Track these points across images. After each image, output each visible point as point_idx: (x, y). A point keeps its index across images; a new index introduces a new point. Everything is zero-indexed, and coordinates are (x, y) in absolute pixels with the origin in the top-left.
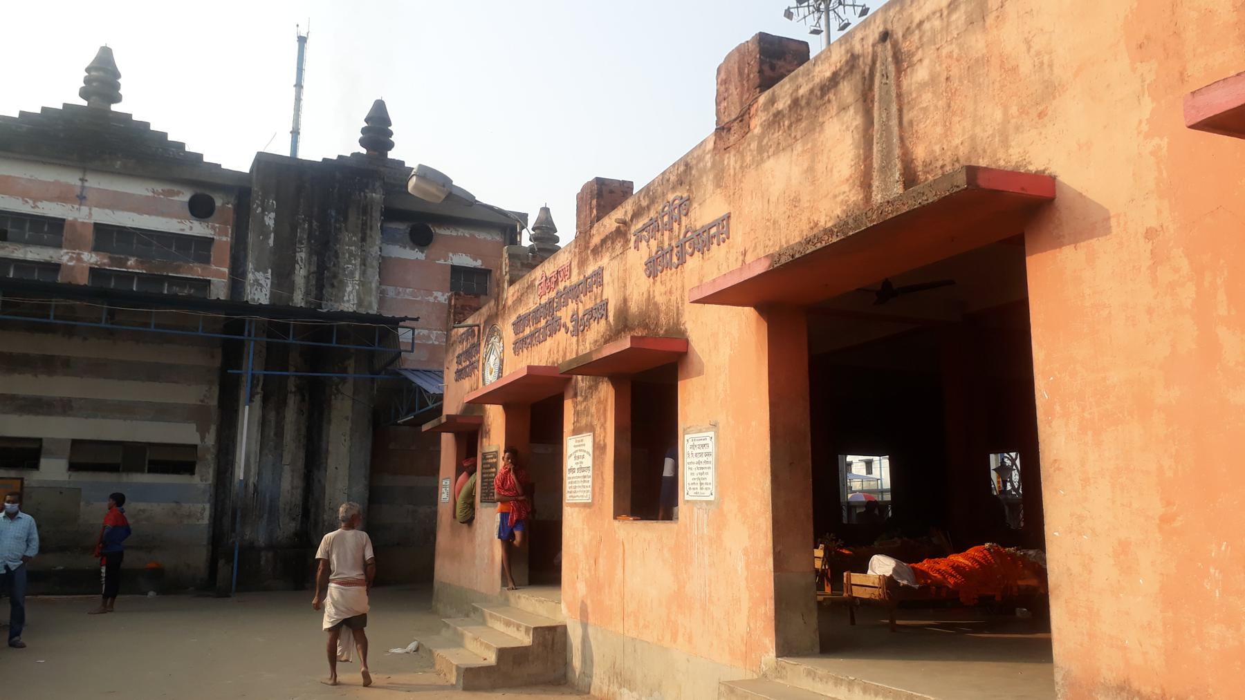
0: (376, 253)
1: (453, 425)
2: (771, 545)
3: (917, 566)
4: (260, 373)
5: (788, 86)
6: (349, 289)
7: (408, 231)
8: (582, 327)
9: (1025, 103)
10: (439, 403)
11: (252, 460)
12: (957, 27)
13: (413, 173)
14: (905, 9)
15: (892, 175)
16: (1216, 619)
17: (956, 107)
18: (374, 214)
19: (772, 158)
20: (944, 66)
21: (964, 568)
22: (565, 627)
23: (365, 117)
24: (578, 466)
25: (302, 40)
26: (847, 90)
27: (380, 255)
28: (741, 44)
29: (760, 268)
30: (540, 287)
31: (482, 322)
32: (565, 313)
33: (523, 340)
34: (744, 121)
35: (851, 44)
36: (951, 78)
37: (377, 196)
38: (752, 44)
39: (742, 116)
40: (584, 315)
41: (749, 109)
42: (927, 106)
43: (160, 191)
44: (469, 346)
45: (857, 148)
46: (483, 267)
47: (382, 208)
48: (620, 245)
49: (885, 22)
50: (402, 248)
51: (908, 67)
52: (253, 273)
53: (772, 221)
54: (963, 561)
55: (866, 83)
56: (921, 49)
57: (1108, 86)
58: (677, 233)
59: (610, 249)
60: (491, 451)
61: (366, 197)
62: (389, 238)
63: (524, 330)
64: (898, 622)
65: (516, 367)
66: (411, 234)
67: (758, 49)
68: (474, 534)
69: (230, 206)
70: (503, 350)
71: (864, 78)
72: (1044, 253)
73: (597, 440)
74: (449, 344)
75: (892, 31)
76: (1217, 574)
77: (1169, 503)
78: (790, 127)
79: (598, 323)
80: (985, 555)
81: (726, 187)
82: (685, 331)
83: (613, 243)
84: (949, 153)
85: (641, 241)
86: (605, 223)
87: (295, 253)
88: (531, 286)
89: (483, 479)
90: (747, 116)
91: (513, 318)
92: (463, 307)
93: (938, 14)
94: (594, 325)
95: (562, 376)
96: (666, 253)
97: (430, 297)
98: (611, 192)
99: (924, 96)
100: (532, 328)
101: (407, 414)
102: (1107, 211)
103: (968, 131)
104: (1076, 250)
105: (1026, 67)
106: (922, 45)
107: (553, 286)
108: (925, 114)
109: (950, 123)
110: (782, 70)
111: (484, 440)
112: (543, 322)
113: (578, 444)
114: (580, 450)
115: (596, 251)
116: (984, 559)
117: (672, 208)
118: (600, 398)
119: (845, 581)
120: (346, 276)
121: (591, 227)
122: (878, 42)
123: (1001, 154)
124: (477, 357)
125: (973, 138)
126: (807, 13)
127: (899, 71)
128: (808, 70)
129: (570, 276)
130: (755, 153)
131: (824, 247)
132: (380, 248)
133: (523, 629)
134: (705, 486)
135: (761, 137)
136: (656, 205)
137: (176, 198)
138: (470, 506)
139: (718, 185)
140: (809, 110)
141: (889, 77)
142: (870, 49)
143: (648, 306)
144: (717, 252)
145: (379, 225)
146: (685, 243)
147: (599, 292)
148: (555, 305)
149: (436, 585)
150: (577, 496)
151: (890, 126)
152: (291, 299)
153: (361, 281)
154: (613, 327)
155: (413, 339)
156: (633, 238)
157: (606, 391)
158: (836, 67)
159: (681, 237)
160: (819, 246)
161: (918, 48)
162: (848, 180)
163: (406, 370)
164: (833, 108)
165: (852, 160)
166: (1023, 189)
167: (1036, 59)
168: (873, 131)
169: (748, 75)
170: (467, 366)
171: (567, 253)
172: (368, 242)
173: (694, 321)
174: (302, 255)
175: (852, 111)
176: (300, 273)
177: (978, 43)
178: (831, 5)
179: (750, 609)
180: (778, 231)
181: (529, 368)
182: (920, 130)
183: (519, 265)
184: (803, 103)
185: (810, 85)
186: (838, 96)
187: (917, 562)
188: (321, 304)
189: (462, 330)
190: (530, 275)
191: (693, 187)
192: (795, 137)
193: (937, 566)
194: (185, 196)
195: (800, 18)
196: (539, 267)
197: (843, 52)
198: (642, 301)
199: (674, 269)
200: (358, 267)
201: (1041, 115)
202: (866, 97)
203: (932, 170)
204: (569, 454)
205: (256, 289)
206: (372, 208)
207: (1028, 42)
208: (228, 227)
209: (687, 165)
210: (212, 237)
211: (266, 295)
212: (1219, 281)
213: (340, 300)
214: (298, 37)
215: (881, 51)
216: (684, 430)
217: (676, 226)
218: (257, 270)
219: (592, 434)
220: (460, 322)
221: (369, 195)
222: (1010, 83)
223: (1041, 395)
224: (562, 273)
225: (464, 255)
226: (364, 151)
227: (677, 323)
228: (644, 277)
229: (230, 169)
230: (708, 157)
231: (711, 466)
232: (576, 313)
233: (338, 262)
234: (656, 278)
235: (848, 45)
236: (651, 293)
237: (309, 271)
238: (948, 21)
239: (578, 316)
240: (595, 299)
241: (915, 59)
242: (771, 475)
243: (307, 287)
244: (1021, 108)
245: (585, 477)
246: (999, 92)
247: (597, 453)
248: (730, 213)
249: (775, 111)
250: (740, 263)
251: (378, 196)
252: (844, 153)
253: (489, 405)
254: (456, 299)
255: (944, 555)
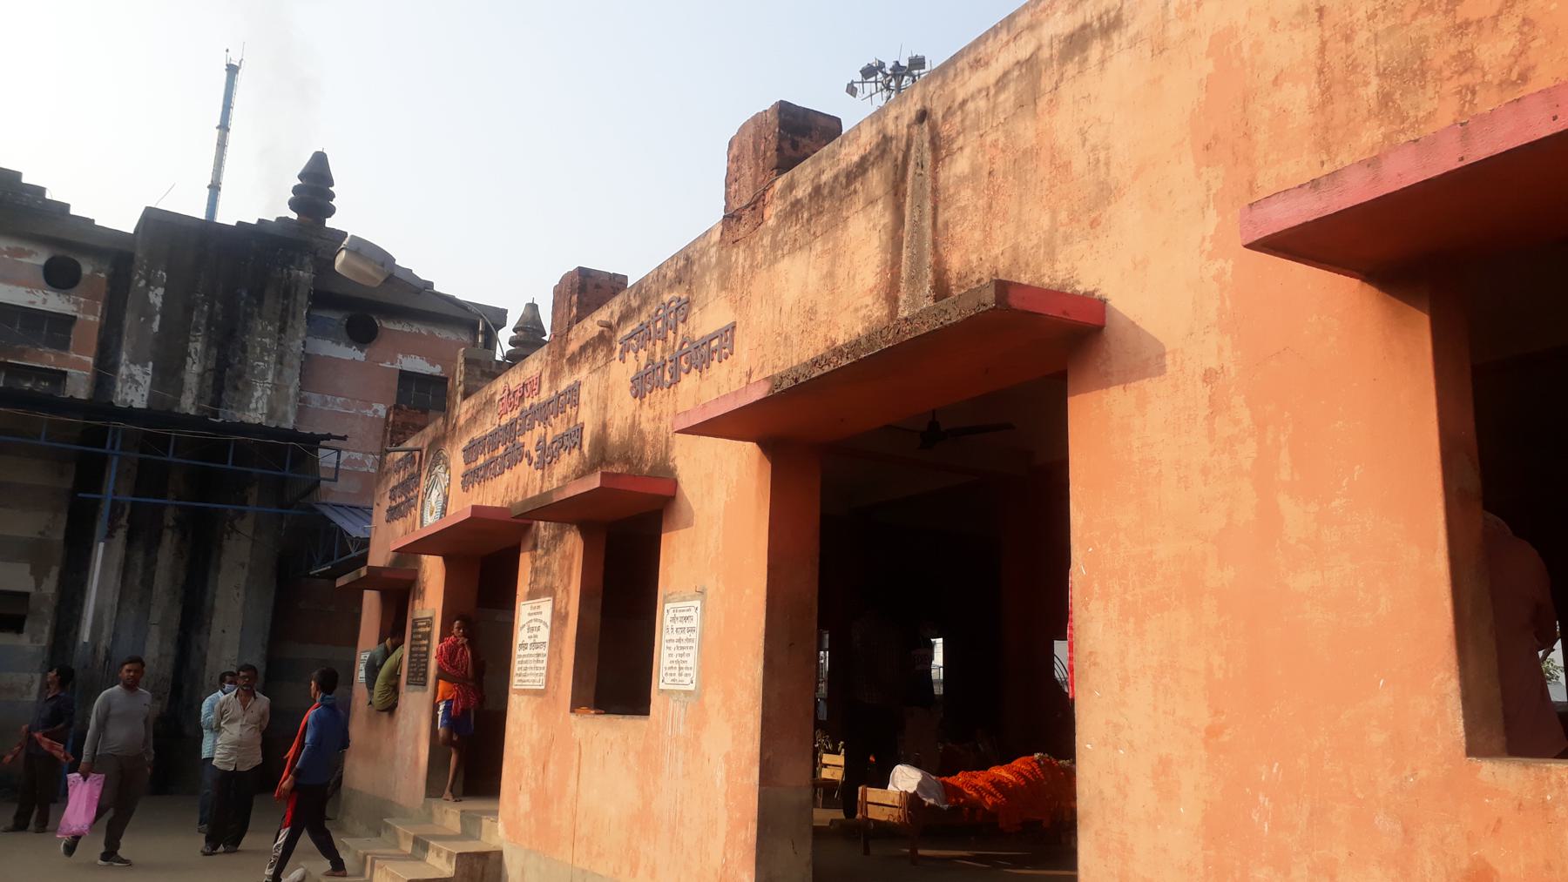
0: (298, 348)
1: (376, 579)
2: (758, 750)
3: (950, 780)
4: (126, 498)
5: (809, 170)
6: (257, 394)
7: (344, 323)
8: (549, 458)
9: (1076, 208)
10: (364, 551)
11: (106, 618)
12: (1004, 111)
13: (342, 246)
14: (948, 83)
15: (921, 288)
16: (1263, 860)
17: (998, 208)
18: (299, 297)
19: (786, 258)
20: (987, 157)
21: (1006, 784)
22: (500, 853)
23: (299, 172)
24: (532, 641)
25: (232, 70)
26: (876, 179)
27: (303, 352)
28: (757, 114)
29: (758, 394)
30: (501, 403)
31: (426, 445)
32: (529, 439)
33: (475, 472)
34: (756, 210)
35: (883, 123)
36: (995, 173)
37: (305, 275)
38: (771, 114)
39: (756, 202)
40: (553, 443)
41: (764, 195)
42: (966, 205)
43: (5, 249)
44: (406, 477)
45: (884, 251)
46: (442, 375)
47: (311, 290)
48: (602, 354)
49: (923, 98)
50: (334, 344)
51: (945, 157)
52: (127, 366)
53: (783, 335)
54: (1006, 775)
55: (899, 172)
56: (962, 135)
57: (1170, 192)
58: (672, 343)
59: (590, 359)
60: (425, 616)
61: (289, 275)
62: (317, 329)
63: (477, 459)
64: (921, 852)
65: (460, 509)
66: (348, 326)
67: (777, 122)
68: (396, 725)
69: (102, 275)
70: (449, 484)
71: (896, 166)
72: (1088, 394)
73: (558, 607)
74: (382, 472)
75: (931, 109)
76: (1266, 804)
77: (1217, 713)
78: (809, 220)
79: (569, 454)
80: (1033, 768)
81: (732, 290)
82: (675, 469)
83: (594, 351)
84: (988, 265)
85: (628, 352)
86: (585, 326)
87: (188, 343)
88: (490, 401)
89: (411, 653)
90: (761, 203)
91: (465, 443)
92: (405, 426)
93: (984, 93)
94: (564, 456)
95: (514, 520)
96: (658, 368)
97: (367, 411)
98: (598, 286)
99: (962, 193)
100: (487, 457)
101: (323, 563)
102: (1162, 345)
103: (1011, 239)
104: (1125, 391)
105: (1079, 164)
106: (964, 130)
107: (517, 403)
108: (962, 214)
109: (991, 228)
110: (807, 150)
111: (417, 601)
112: (501, 450)
113: (533, 611)
114: (536, 620)
115: (573, 361)
116: (1032, 773)
117: (668, 311)
118: (565, 552)
119: (859, 798)
120: (255, 376)
121: (569, 330)
122: (915, 123)
123: (1046, 270)
124: (415, 492)
125: (1015, 248)
126: (874, 91)
127: (936, 160)
128: (834, 151)
129: (539, 390)
130: (768, 249)
131: (833, 371)
132: (304, 343)
133: (444, 855)
134: (685, 672)
135: (776, 231)
136: (649, 307)
137: (25, 260)
138: (393, 689)
139: (723, 288)
140: (832, 202)
141: (925, 166)
142: (906, 130)
143: (631, 436)
144: (718, 370)
145: (305, 312)
146: (681, 356)
147: (574, 413)
148: (518, 427)
149: (344, 792)
150: (528, 681)
151: (922, 227)
152: (178, 403)
153: (275, 384)
154: (587, 460)
155: (338, 463)
156: (619, 347)
157: (574, 543)
158: (865, 150)
159: (677, 348)
160: (827, 369)
161: (958, 134)
162: (871, 291)
163: (326, 504)
164: (859, 201)
165: (878, 267)
166: (1065, 313)
167: (1091, 155)
168: (903, 232)
169: (765, 153)
170: (402, 503)
171: (537, 361)
172: (288, 333)
173: (685, 457)
174: (196, 346)
175: (880, 206)
176: (193, 370)
177: (1027, 131)
178: (904, 83)
179: (728, 834)
180: (790, 349)
181: (474, 507)
182: (956, 234)
183: (478, 373)
184: (826, 191)
185: (835, 171)
186: (866, 187)
187: (949, 776)
188: (217, 412)
189: (400, 455)
190: (490, 387)
191: (694, 287)
192: (815, 233)
193: (975, 781)
194: (40, 258)
195: (865, 96)
196: (501, 378)
197: (874, 132)
198: (626, 428)
199: (665, 390)
200: (272, 366)
201: (1094, 224)
202: (897, 190)
203: (967, 284)
204: (521, 624)
205: (130, 387)
206: (297, 290)
207: (1083, 133)
208: (98, 302)
209: (687, 259)
210: (73, 314)
211: (143, 395)
212: (1283, 439)
213: (244, 407)
214: (227, 65)
215: (918, 134)
216: (665, 597)
217: (671, 334)
218: (133, 361)
219: (551, 598)
220: (398, 445)
221: (294, 272)
222: (1061, 182)
223: (1078, 569)
224: (529, 386)
225: (418, 357)
226: (294, 216)
227: (666, 459)
228: (629, 397)
229: (106, 226)
230: (714, 250)
231: (693, 645)
232: (542, 440)
233: (246, 357)
234: (644, 400)
235: (880, 123)
236: (637, 419)
237: (204, 367)
238: (995, 102)
239: (545, 445)
240: (568, 422)
241: (955, 146)
242: (765, 659)
243: (200, 388)
244: (1072, 214)
245: (538, 655)
246: (1048, 192)
247: (557, 624)
248: (735, 323)
249: (793, 199)
250: (744, 385)
251: (306, 275)
252: (869, 257)
253: (426, 556)
254: (396, 414)
255: (984, 766)
